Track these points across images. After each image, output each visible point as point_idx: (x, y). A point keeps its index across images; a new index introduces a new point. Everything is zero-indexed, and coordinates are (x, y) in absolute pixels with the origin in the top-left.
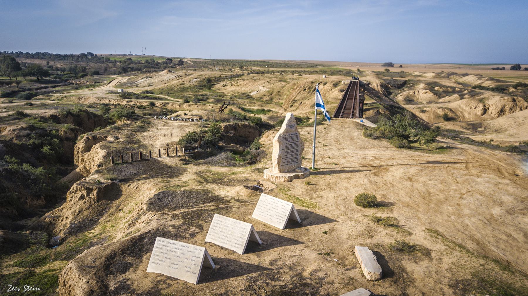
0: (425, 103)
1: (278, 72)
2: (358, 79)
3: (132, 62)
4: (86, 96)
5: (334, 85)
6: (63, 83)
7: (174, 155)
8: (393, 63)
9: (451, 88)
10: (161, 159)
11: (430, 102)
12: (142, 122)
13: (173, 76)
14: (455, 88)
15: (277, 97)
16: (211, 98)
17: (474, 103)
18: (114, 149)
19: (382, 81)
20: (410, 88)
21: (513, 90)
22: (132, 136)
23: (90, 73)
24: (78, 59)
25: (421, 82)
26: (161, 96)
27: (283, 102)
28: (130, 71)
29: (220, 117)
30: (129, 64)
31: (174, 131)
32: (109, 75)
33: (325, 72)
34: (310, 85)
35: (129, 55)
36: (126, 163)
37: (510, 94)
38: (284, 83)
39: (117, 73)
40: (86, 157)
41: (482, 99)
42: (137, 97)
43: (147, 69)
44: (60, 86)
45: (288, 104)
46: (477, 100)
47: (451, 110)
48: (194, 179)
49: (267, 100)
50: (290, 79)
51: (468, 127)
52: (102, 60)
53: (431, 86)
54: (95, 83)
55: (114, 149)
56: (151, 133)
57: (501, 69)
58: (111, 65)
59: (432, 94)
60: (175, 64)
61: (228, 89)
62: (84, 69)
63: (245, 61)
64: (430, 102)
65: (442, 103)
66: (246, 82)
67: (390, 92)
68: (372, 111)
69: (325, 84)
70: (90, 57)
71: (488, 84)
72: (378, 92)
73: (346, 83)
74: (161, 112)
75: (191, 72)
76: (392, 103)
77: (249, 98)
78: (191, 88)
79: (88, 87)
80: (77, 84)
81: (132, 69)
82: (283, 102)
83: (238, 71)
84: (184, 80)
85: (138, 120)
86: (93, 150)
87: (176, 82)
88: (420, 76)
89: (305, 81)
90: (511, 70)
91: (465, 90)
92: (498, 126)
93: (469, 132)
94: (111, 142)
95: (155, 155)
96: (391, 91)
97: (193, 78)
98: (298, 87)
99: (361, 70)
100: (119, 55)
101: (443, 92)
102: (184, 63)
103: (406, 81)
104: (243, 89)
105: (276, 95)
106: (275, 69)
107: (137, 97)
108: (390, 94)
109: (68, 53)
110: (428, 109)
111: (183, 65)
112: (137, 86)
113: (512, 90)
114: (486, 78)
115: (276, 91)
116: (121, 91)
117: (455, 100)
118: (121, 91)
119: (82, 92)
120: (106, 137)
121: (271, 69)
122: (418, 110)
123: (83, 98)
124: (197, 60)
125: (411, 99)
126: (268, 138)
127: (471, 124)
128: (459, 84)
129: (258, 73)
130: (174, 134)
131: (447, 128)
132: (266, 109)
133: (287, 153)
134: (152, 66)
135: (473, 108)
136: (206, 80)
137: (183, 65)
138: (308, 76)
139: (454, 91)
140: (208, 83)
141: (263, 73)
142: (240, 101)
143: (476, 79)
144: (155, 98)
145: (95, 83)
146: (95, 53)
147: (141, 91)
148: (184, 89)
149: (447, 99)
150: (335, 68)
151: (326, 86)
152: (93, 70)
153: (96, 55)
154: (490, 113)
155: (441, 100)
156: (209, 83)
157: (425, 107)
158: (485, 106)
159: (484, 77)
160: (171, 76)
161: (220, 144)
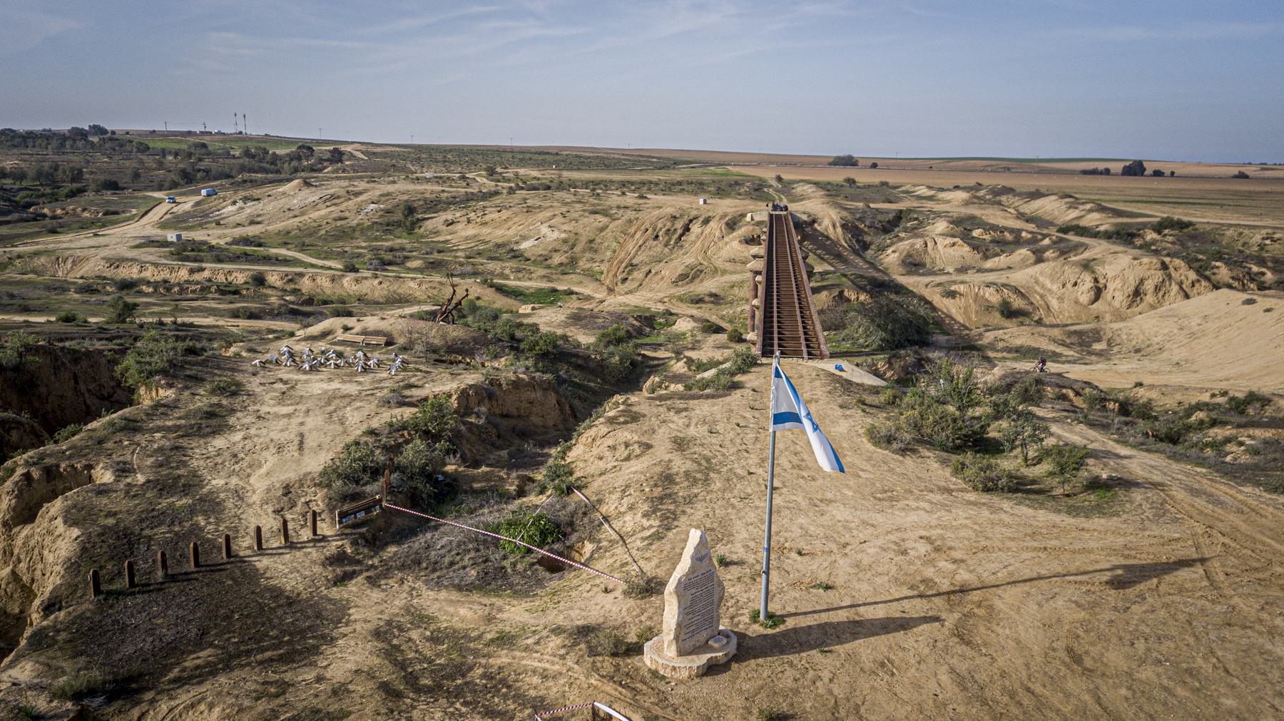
0: (951, 270)
1: (586, 184)
2: (786, 208)
3: (209, 154)
4: (78, 253)
5: (727, 224)
6: (16, 216)
7: (306, 534)
8: (855, 155)
9: (1011, 231)
10: (262, 563)
11: (962, 270)
12: (213, 392)
13: (316, 198)
14: (1020, 231)
15: (588, 255)
16: (416, 258)
17: (1071, 273)
18: (111, 521)
19: (845, 214)
20: (914, 232)
21: (1155, 236)
22: (177, 456)
23: (93, 186)
24: (62, 145)
25: (938, 215)
26: (283, 252)
27: (604, 267)
28: (203, 180)
29: (444, 337)
30: (200, 160)
31: (311, 422)
32: (146, 189)
33: (699, 187)
34: (669, 224)
35: (202, 133)
36: (146, 588)
37: (1146, 247)
38: (605, 220)
39: (167, 184)
40: (19, 542)
41: (1089, 261)
42: (220, 255)
43: (246, 176)
44: (8, 222)
45: (615, 275)
46: (1075, 264)
47: (1016, 290)
48: (370, 675)
49: (561, 264)
50: (619, 207)
51: (1068, 341)
52: (128, 147)
53: (963, 227)
54: (106, 214)
55: (111, 521)
56: (238, 437)
57: (1101, 173)
58: (149, 161)
59: (967, 248)
60: (321, 160)
61: (459, 232)
62: (77, 176)
63: (499, 151)
64: (962, 270)
65: (992, 270)
66: (505, 214)
67: (865, 242)
68: (825, 293)
69: (707, 221)
70: (95, 139)
71: (1092, 219)
72: (835, 243)
73: (757, 218)
74: (281, 305)
75: (362, 185)
76: (872, 273)
77: (515, 257)
78: (361, 229)
79: (84, 226)
80: (54, 217)
81: (208, 175)
82: (604, 267)
83: (483, 182)
84: (343, 207)
85: (198, 380)
86: (41, 523)
87: (322, 212)
88: (930, 198)
89: (656, 212)
90: (1123, 174)
91: (1045, 236)
92: (1141, 337)
93: (1072, 353)
94: (103, 491)
95: (244, 544)
96: (868, 239)
97: (370, 199)
98: (638, 229)
99: (785, 177)
100: (174, 134)
101: (993, 241)
102: (345, 157)
103: (901, 211)
104: (499, 232)
105: (584, 251)
106: (575, 175)
107: (220, 255)
108: (866, 247)
109: (37, 127)
110: (961, 288)
111: (341, 161)
112: (218, 224)
113: (1151, 236)
114: (1088, 206)
115: (583, 240)
116: (174, 239)
117: (1024, 264)
118: (174, 239)
119: (66, 241)
120: (89, 467)
121: (567, 174)
122: (938, 289)
123: (70, 260)
124: (379, 150)
125: (918, 260)
126: (595, 451)
127: (1075, 332)
128: (1029, 220)
129: (535, 189)
130: (310, 442)
131: (1018, 342)
132: (560, 288)
133: (693, 612)
134: (261, 164)
135: (1069, 286)
136: (402, 207)
137: (341, 161)
138: (660, 198)
139: (1018, 242)
140: (406, 216)
141: (549, 188)
142: (492, 266)
143: (1064, 207)
144: (267, 260)
145: (106, 214)
146: (109, 128)
147: (229, 239)
148: (344, 234)
149: (1002, 260)
150: (719, 170)
151: (708, 229)
152: (102, 177)
153: (113, 133)
154: (1109, 297)
155: (989, 264)
156: (409, 216)
157: (954, 282)
158: (1096, 280)
159: (1083, 204)
160: (310, 196)
161: (450, 468)
